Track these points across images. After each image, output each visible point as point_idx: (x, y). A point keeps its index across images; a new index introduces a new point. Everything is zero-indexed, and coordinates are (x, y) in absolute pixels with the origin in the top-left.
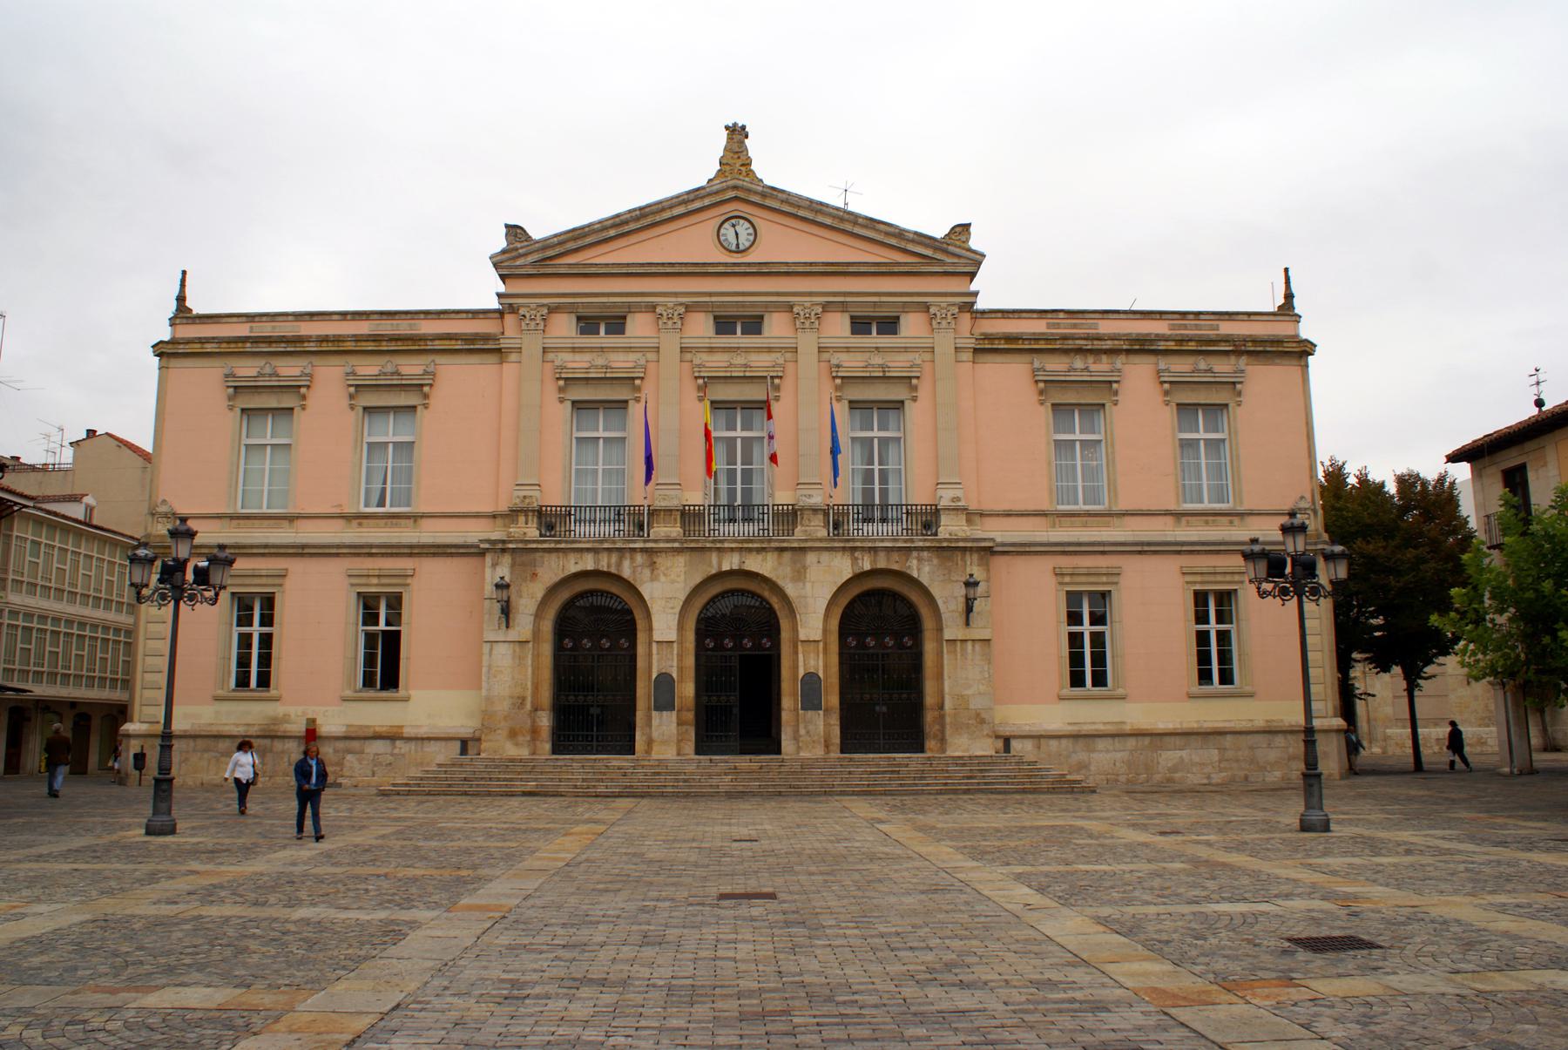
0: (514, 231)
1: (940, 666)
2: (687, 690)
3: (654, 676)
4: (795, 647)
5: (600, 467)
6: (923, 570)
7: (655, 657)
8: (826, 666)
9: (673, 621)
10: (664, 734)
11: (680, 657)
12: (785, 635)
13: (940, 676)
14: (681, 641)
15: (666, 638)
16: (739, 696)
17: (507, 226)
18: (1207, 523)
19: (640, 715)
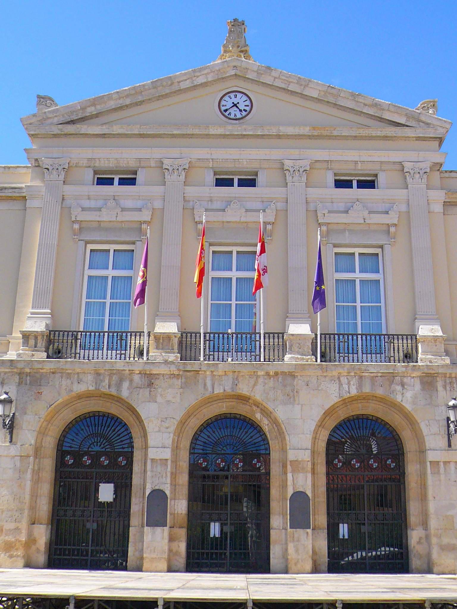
0: (43, 100)
1: (423, 486)
2: (179, 506)
3: (148, 492)
4: (284, 466)
5: (108, 301)
6: (408, 397)
7: (149, 474)
8: (314, 485)
9: (168, 439)
10: (297, 542)
11: (174, 475)
12: (274, 455)
13: (424, 498)
14: (175, 460)
15: (161, 460)
16: (229, 522)
17: (39, 97)
18: (74, 137)
19: (132, 531)
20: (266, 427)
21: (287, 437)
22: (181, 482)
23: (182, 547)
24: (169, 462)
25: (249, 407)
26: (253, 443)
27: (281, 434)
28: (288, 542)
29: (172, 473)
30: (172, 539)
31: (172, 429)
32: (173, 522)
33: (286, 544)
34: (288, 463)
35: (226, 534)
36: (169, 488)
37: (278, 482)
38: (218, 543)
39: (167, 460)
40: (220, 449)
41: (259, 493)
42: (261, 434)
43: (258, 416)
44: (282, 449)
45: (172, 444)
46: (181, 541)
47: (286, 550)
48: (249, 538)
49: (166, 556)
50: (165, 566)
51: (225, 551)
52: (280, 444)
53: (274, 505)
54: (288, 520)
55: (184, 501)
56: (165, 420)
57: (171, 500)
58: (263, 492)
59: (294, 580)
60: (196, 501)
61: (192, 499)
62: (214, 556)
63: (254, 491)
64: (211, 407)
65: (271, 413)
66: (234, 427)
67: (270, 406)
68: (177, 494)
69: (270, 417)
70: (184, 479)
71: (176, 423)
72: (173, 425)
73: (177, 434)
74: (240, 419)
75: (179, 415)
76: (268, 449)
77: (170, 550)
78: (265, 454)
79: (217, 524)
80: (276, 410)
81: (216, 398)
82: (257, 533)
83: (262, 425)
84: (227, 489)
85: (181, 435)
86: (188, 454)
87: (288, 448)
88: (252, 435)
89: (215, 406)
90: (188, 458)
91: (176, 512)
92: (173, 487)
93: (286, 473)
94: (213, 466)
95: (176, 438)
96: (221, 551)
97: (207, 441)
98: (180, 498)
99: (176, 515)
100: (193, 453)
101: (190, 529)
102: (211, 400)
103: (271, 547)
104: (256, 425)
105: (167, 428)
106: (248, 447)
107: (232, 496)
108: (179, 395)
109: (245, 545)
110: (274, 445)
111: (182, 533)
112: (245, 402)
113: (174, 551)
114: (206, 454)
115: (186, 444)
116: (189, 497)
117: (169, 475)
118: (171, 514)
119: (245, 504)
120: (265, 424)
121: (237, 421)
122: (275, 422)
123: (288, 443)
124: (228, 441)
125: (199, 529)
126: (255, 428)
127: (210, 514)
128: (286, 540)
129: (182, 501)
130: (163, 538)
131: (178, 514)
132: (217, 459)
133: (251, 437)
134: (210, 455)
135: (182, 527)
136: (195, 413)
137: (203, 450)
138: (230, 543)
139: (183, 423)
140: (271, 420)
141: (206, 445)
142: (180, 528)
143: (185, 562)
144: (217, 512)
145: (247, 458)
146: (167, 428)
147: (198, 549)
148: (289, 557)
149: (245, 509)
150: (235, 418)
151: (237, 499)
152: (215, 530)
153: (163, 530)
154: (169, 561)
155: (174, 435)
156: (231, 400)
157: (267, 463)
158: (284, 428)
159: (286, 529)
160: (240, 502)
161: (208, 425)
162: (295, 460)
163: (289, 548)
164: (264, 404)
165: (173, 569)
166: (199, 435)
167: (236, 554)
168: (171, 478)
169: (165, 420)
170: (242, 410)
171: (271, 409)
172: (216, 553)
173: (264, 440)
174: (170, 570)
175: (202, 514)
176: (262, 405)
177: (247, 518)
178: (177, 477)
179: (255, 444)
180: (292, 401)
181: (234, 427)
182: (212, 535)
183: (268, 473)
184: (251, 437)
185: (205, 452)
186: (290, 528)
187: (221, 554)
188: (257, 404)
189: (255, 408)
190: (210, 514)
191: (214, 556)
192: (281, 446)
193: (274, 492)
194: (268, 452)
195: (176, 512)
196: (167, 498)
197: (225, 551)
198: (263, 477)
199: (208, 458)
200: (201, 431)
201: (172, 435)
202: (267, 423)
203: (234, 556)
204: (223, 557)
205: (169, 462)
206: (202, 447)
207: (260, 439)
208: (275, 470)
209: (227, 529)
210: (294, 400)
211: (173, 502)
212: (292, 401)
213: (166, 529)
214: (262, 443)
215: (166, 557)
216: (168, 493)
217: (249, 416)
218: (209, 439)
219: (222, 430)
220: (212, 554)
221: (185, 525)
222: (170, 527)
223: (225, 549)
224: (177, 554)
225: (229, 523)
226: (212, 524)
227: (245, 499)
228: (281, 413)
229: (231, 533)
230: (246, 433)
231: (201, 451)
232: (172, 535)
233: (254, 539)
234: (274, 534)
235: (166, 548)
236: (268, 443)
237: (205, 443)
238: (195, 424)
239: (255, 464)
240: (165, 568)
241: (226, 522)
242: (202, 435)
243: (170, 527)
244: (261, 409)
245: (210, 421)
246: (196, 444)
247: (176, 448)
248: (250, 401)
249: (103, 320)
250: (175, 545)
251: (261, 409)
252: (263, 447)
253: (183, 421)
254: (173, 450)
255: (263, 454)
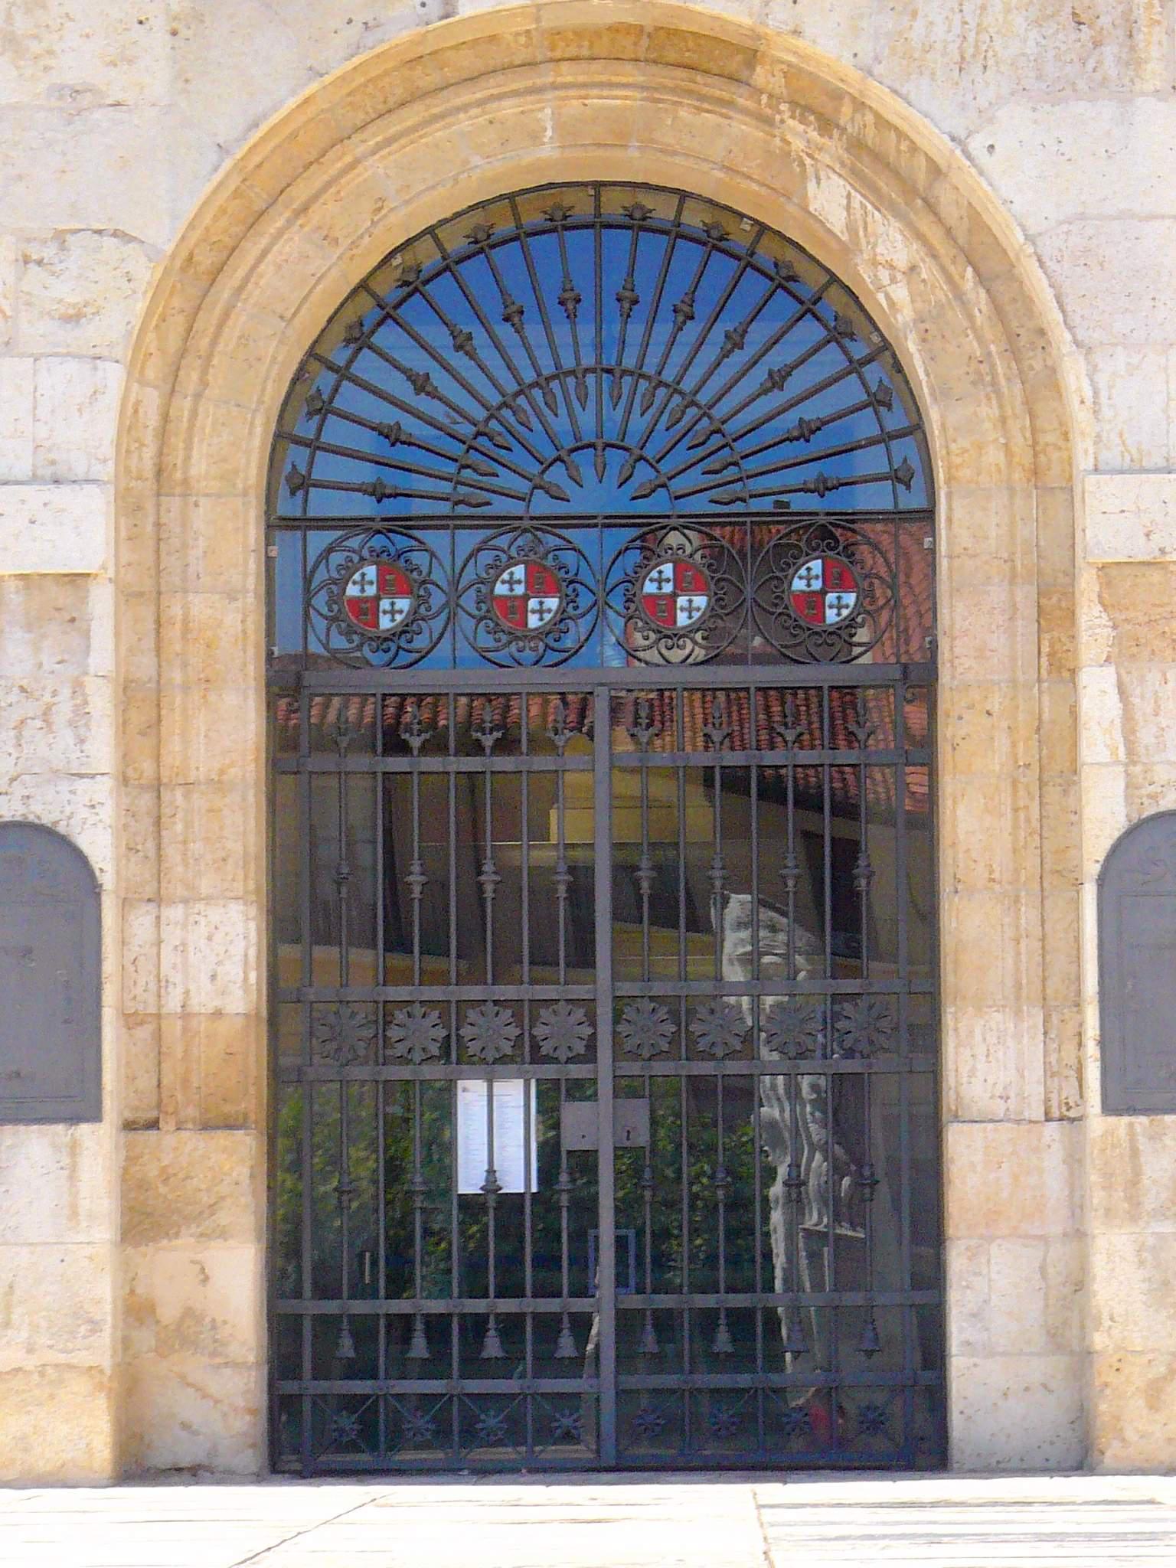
4: (1054, 612)
11: (144, 710)
12: (972, 528)
20: (900, 293)
21: (1074, 375)
22: (202, 763)
23: (230, 1280)
24: (102, 601)
25: (753, 132)
26: (789, 421)
27: (1021, 340)
28: (1096, 1226)
29: (127, 690)
30: (143, 1219)
31: (119, 318)
32: (147, 1083)
33: (1078, 1235)
34: (1087, 583)
35: (585, 1163)
36: (107, 813)
37: (1003, 742)
38: (528, 1236)
39: (76, 580)
40: (522, 486)
41: (847, 852)
42: (859, 351)
43: (828, 206)
44: (1035, 472)
45: (124, 450)
46: (223, 1234)
47: (1079, 1284)
48: (777, 1217)
49: (100, 1351)
50: (89, 1431)
51: (579, 1305)
52: (1019, 426)
53: (983, 928)
54: (1092, 1050)
55: (236, 910)
56: (49, 252)
57: (126, 904)
58: (879, 849)
59: (1147, 1511)
60: (324, 937)
61: (300, 915)
62: (492, 1347)
63: (811, 839)
64: (438, 134)
65: (936, 171)
66: (629, 302)
67: (929, 115)
68: (172, 852)
69: (931, 207)
70: (228, 732)
71: (146, 274)
72: (120, 296)
73: (153, 371)
74: (676, 233)
75: (166, 210)
76: (914, 473)
77: (136, 1310)
78: (898, 516)
79: (513, 1097)
80: (977, 145)
81: (468, 61)
82: (838, 1170)
83: (862, 274)
84: (586, 811)
85: (190, 378)
86: (254, 533)
87: (1084, 462)
88: (777, 359)
89: (464, 123)
90: (254, 566)
91: (173, 1003)
92: (146, 801)
93: (1061, 668)
94: (466, 623)
95: (152, 400)
96: (550, 1305)
97: (412, 426)
98: (205, 886)
99: (173, 1030)
100: (289, 524)
101: (294, 1157)
102: (427, 79)
103: (957, 1261)
104: (813, 281)
105: (74, 318)
106: (751, 465)
107: (625, 871)
108: (157, 39)
109: (742, 1252)
110: (966, 440)
111: (230, 1170)
112: (718, 89)
113: (168, 1313)
114: (404, 525)
115: (232, 445)
116: (273, 874)
117: (102, 701)
118: (131, 1020)
119: (735, 942)
120: (890, 272)
121: (653, 247)
122: (976, 251)
123: (1081, 417)
124: (587, 420)
125: (364, 1164)
126: (809, 309)
127: (454, 1013)
128: (1077, 1208)
129: (215, 914)
130: (74, 1214)
131: (186, 1015)
132: (497, 568)
133: (777, 380)
134: (436, 539)
135: (230, 1125)
136: (300, 192)
137: (379, 493)
138: (621, 1243)
139: (202, 276)
140: (935, 235)
141: (403, 454)
142: (206, 1126)
143: (261, 1400)
144: (508, 992)
145: (747, 556)
146: (74, 318)
147: (361, 1291)
148: (1099, 1340)
149: (734, 974)
150: (638, 223)
151: (669, 903)
152: (493, 1134)
153: (74, 1148)
154: (129, 1392)
155: (136, 371)
156: (597, 72)
157: (905, 593)
158: (1044, 295)
159: (1071, 1119)
160: (698, 924)
161: (410, 289)
162: (1143, 551)
163: (1099, 1265)
164: (879, 96)
165: (162, 1458)
166: (343, 373)
167: (665, 1322)
168: (123, 726)
169: (49, 252)
170: (698, 151)
171: (935, 141)
172: (511, 1326)
173: (878, 401)
174: (138, 1465)
175: (386, 1012)
176: (860, 106)
177: (749, 1039)
178: (172, 721)
179: (806, 432)
180: (1110, 68)
181: (629, 302)
182: (469, 1181)
183: (919, 679)
184: (777, 380)
185: (393, 508)
186: (1110, 1108)
187: (547, 1326)
188: (819, 103)
189: (798, 134)
190: (454, 1013)
191: (492, 1347)
192: (1020, 444)
193: (973, 824)
194: (912, 500)
195: (173, 1003)
196: (95, 890)
197: (579, 1305)
198: (878, 708)
199: (420, 559)
200: (322, 409)
201: (114, 375)
202: (902, 260)
203: (649, 1341)
204: (566, 1345)
205: (102, 601)
206: (366, 473)
207: (850, 391)
208: (976, 636)
209: (590, 1125)
210: (1133, 61)
211: (142, 923)
212: (1110, 68)
213: (97, 1143)
214: (865, 425)
215: (106, 1362)
216: (99, 846)
217: (746, 196)
218: (423, 404)
219: (534, 332)
220: (476, 1325)
221: (253, 1099)
222: (129, 1126)
223: (582, 1290)
224: (190, 1332)
225: (605, 1087)
226: (471, 1096)
227: (738, 904)
228: (1021, 169)
229: (632, 1163)
230: (735, 341)
231: (363, 506)
232: (143, 1185)
233: (813, 1219)
234: (970, 1162)
235: (102, 1293)
236: (916, 429)
237: (392, 436)
238: (303, 278)
239: (815, 601)
240: (101, 1450)
241: (577, 1071)
242: (368, 366)
243: (129, 1126)
244: (856, 145)
245: (428, 257)
246: (314, 445)
247: (151, 491)
248: (760, 76)
249: (420, 840)
250: (168, 1268)
251: (856, 145)
252: (872, 461)
253: (206, 260)
254: (127, 505)
255: (870, 516)
